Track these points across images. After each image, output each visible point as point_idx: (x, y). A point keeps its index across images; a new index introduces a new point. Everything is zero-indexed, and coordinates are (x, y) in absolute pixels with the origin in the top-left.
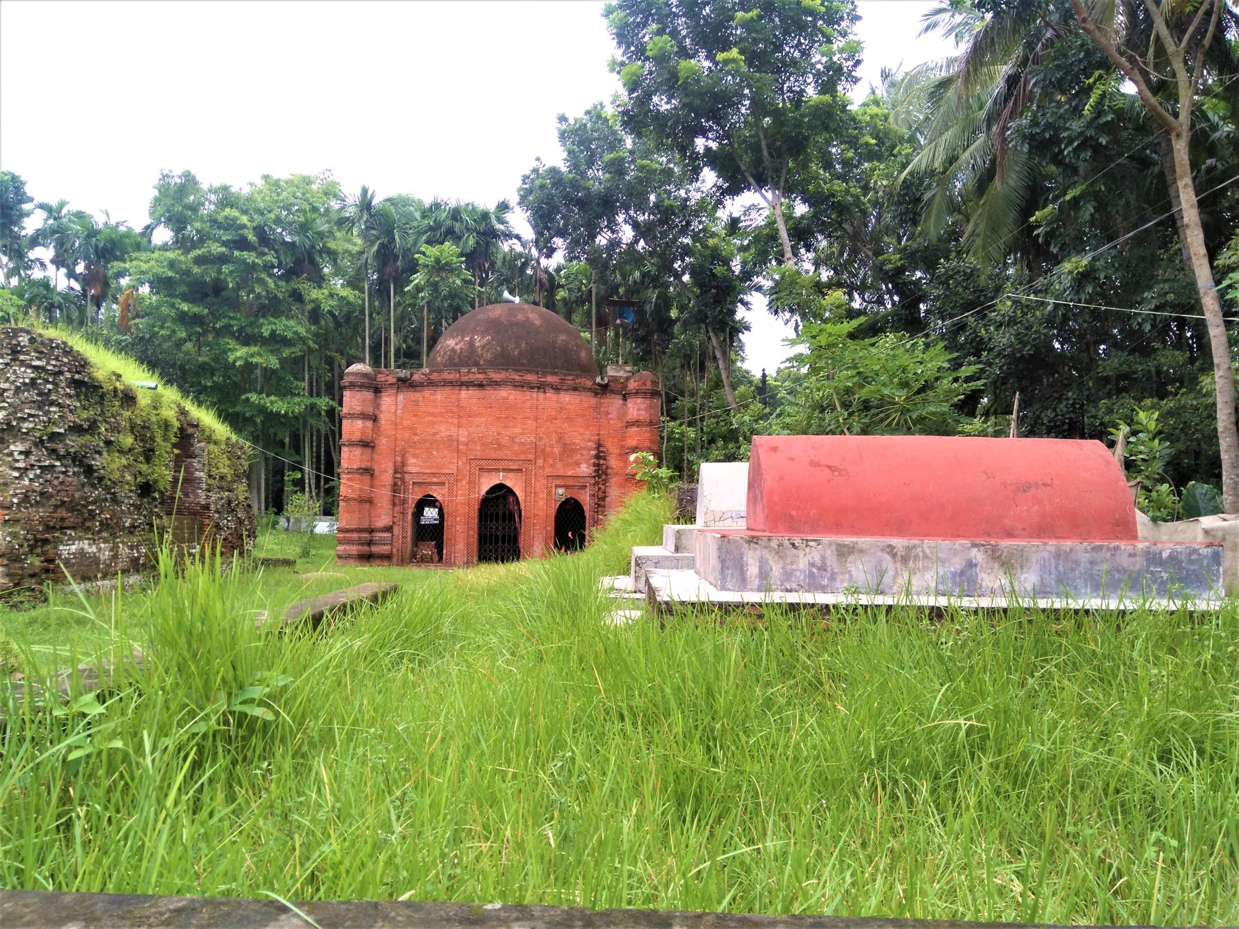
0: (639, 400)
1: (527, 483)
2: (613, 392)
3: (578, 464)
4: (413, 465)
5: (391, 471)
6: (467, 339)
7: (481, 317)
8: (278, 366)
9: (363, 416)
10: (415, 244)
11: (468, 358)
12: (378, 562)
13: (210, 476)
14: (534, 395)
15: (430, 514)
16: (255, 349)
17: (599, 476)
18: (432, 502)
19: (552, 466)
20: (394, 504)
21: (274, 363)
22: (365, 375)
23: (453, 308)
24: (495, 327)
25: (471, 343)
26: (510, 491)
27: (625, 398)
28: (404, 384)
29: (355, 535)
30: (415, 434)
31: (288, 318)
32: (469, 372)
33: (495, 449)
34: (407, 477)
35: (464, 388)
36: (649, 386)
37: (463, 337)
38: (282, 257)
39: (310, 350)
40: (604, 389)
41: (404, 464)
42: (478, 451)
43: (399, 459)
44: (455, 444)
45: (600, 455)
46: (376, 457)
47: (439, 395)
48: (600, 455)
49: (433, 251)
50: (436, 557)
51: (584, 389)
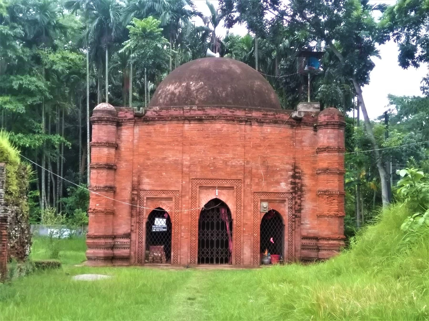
0: (329, 131)
1: (238, 198)
2: (306, 124)
3: (278, 183)
4: (147, 184)
5: (129, 189)
6: (184, 84)
7: (194, 67)
8: (24, 111)
9: (109, 145)
10: (125, 18)
11: (186, 99)
12: (119, 263)
13: (6, 192)
14: (243, 127)
15: (160, 223)
16: (7, 98)
17: (295, 192)
18: (159, 213)
19: (258, 184)
20: (132, 216)
21: (21, 108)
22: (109, 112)
23: (155, 68)
24: (205, 75)
25: (188, 88)
26: (224, 205)
27: (315, 129)
28: (140, 119)
29: (102, 241)
30: (149, 159)
31: (31, 76)
32: (191, 109)
33: (212, 171)
34: (142, 194)
35: (187, 122)
36: (336, 119)
37: (181, 83)
38: (27, 30)
39: (47, 100)
40: (298, 122)
41: (139, 183)
42: (198, 172)
43: (135, 179)
44: (180, 167)
45: (296, 175)
46: (117, 177)
47: (167, 128)
48: (296, 175)
49: (139, 23)
50: (164, 259)
51: (283, 122)
